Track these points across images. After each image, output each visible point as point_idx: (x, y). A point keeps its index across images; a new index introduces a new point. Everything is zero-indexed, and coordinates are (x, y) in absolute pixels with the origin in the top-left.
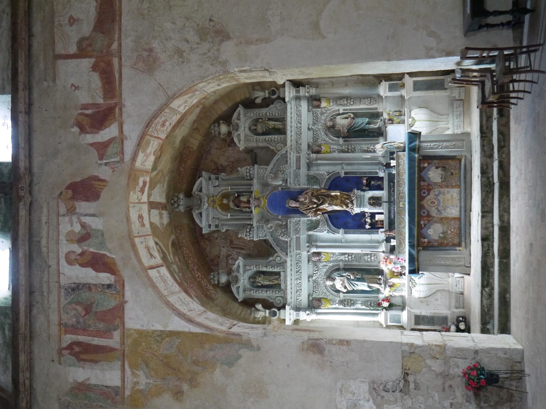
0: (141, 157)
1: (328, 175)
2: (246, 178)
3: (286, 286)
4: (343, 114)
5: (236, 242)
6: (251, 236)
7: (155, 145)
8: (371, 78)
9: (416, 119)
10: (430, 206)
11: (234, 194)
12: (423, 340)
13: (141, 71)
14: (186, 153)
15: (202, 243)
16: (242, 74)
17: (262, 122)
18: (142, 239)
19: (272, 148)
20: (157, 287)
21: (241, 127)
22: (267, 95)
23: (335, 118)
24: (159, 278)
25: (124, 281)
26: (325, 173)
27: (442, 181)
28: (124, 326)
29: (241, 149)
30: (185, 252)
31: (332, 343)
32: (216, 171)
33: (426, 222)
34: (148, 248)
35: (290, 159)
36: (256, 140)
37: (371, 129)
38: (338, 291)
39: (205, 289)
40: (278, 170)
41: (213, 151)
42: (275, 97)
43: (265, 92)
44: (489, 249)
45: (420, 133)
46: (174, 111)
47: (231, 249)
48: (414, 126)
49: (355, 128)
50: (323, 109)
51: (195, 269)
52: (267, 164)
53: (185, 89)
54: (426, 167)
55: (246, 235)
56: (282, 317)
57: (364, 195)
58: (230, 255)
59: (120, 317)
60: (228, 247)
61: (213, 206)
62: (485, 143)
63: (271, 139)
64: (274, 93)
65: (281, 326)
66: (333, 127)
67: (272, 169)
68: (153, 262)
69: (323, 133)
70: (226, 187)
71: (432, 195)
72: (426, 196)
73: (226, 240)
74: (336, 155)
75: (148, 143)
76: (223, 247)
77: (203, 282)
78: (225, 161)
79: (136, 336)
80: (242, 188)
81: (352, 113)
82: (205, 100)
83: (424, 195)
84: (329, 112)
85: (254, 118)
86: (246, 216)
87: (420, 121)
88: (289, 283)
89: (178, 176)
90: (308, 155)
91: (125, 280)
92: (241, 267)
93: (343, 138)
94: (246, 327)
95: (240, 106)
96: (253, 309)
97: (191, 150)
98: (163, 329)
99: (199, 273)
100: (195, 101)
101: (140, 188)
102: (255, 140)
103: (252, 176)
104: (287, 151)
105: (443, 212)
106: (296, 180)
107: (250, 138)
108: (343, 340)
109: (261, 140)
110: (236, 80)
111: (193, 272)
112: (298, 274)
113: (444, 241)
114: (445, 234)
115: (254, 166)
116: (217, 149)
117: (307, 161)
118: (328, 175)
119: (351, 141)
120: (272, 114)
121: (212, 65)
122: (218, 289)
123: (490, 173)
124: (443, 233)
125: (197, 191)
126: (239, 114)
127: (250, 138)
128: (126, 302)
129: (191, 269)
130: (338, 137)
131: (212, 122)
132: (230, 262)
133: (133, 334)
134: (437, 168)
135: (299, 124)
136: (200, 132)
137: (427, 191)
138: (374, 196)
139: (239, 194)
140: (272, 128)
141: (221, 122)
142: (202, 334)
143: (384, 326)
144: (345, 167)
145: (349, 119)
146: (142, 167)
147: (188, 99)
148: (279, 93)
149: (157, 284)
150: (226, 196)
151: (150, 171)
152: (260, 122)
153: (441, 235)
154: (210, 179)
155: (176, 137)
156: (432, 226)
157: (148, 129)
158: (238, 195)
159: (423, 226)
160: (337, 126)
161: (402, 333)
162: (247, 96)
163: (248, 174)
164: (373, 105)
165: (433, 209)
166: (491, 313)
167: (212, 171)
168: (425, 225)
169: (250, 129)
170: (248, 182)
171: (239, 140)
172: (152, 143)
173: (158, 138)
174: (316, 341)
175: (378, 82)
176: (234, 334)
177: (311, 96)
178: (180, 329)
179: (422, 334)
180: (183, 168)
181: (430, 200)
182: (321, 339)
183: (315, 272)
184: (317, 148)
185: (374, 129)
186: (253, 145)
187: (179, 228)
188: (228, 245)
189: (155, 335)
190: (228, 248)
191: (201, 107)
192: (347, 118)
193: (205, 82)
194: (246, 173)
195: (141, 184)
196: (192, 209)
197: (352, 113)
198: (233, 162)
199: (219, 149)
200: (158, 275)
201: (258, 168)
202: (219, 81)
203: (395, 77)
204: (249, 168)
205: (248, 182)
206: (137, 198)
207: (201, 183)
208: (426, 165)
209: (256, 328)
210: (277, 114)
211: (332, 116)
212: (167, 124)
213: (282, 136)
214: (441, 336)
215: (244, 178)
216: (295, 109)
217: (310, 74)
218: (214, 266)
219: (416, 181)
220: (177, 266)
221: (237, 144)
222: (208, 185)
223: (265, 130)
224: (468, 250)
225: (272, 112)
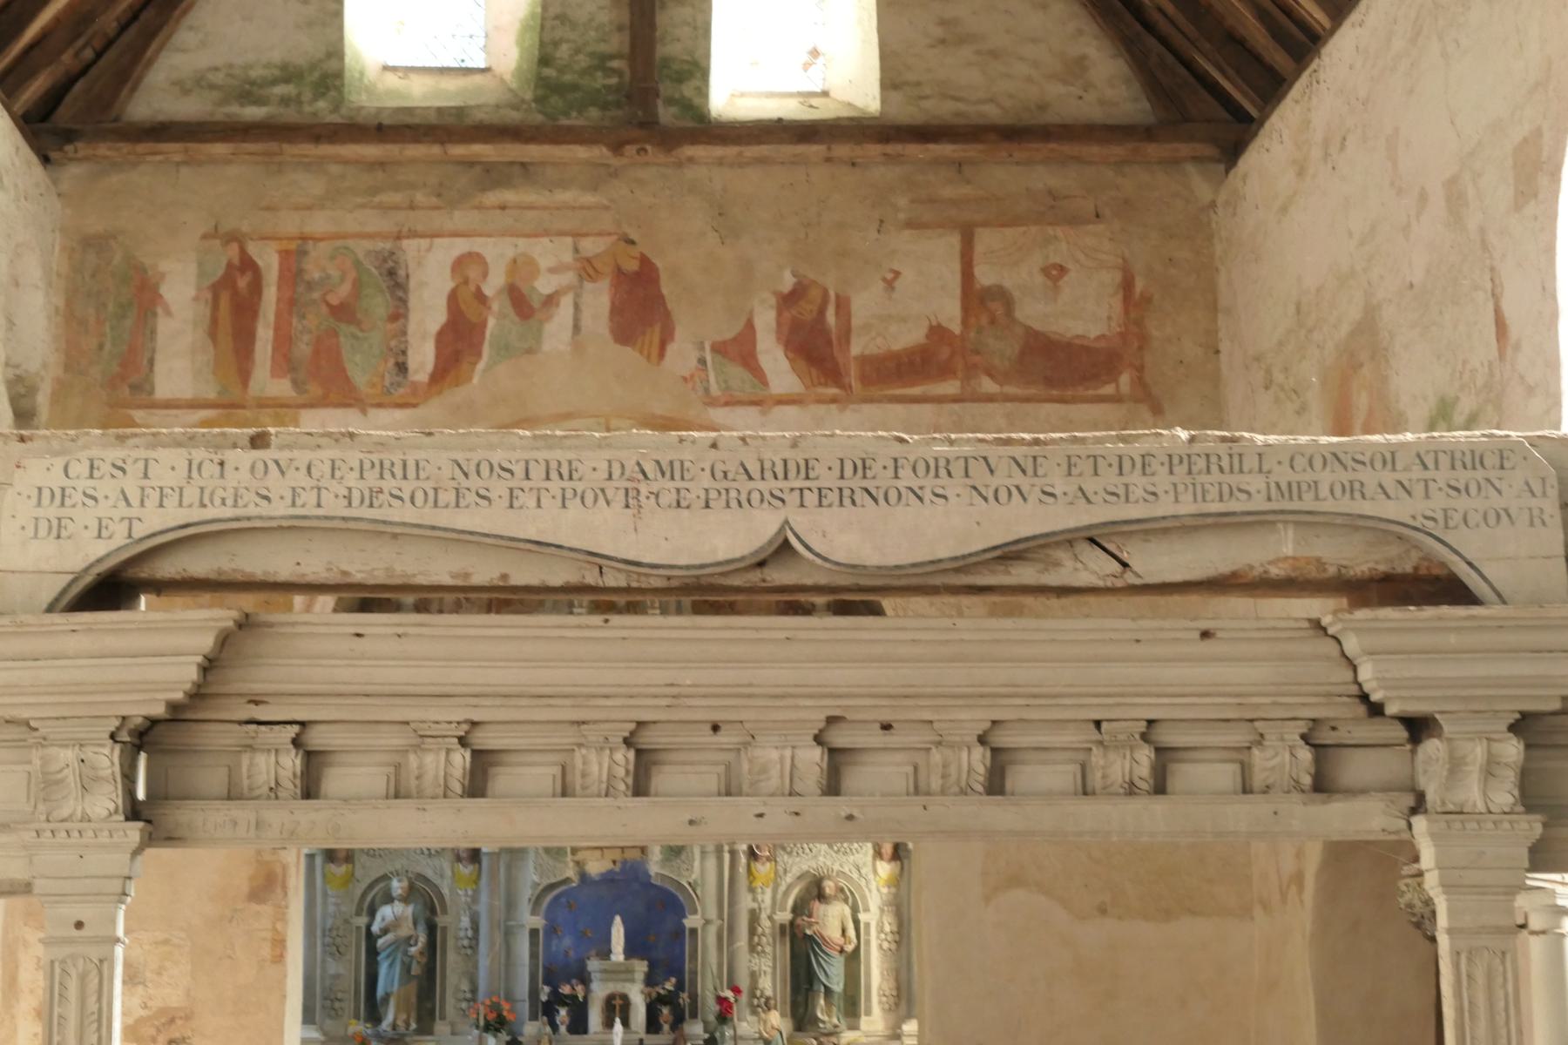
25: (415, 406)
69: (805, 868)
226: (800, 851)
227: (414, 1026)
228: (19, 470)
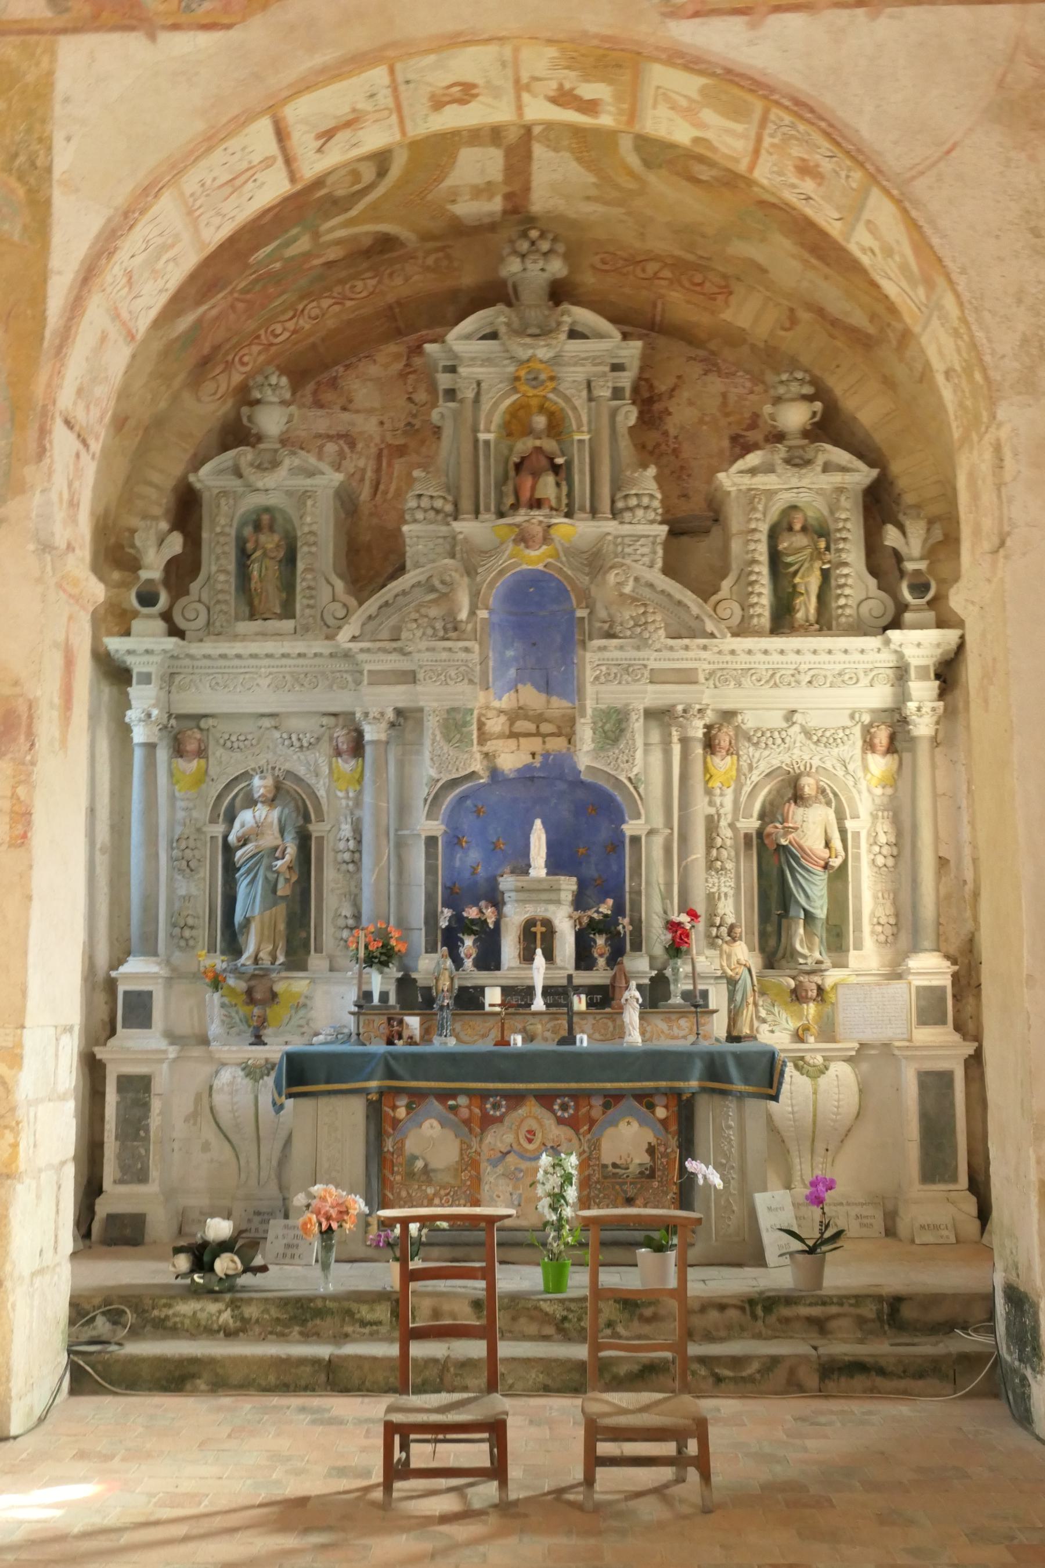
0: (689, 84)
1: (630, 779)
2: (619, 495)
3: (244, 638)
4: (843, 832)
5: (399, 465)
6: (420, 515)
7: (730, 140)
8: (970, 925)
9: (823, 1080)
10: (519, 1127)
11: (563, 454)
12: (38, 1101)
13: (1004, 75)
14: (708, 284)
15: (392, 348)
16: (988, 455)
17: (817, 549)
18: (385, 98)
19: (726, 584)
20: (209, 150)
21: (800, 478)
22: (910, 566)
23: (828, 804)
24: (244, 165)
25: (228, 27)
26: (635, 770)
27: (605, 1166)
28: (64, 31)
29: (721, 476)
30: (360, 284)
31: (20, 782)
32: (646, 395)
33: (464, 1113)
34: (352, 122)
35: (687, 648)
36: (754, 530)
37: (789, 927)
38: (231, 818)
39: (230, 358)
40: (645, 605)
41: (716, 385)
42: (907, 596)
43: (922, 558)
44: (364, 1324)
45: (775, 1098)
46: (854, 211)
47: (373, 450)
48: (796, 1073)
49: (793, 871)
50: (859, 763)
51: (301, 322)
52: (669, 570)
53: (935, 241)
54: (653, 1113)
55: (420, 496)
56: (136, 625)
57: (558, 902)
58: (352, 445)
59: (96, 16)
60: (383, 441)
61: (517, 379)
62: (733, 1314)
63: (756, 581)
64: (920, 588)
65: (83, 607)
66: (798, 797)
67: (651, 586)
68: (303, 141)
69: (776, 763)
70: (590, 422)
71: (557, 1132)
72: (553, 1112)
73: (405, 433)
74: (701, 808)
75: (736, 112)
76: (382, 423)
77: (255, 349)
79: (30, 78)
80: (582, 482)
81: (845, 862)
82: (894, 343)
83: (556, 1107)
84: (850, 782)
85: (830, 521)
86: (487, 495)
87: (815, 1093)
88: (254, 647)
90: (700, 711)
91: (232, 33)
92: (309, 481)
93: (760, 833)
94: (76, 484)
95: (874, 473)
96: (164, 526)
98: (57, 173)
99: (286, 335)
100: (890, 289)
101: (573, 89)
102: (753, 526)
103: (627, 516)
104: (712, 635)
105: (500, 1169)
106: (614, 670)
107: (760, 507)
108: (29, 824)
109: (752, 546)
110: (965, 439)
111: (291, 314)
112: (288, 677)
113: (398, 1173)
114: (423, 1178)
115: (661, 523)
116: (724, 395)
117: (680, 708)
118: (630, 779)
119: (748, 857)
121: (1025, 341)
122: (230, 403)
123: (626, 1328)
124: (426, 1170)
125: (574, 323)
126: (844, 469)
127: (760, 507)
128: (152, 37)
129: (300, 307)
130: (762, 816)
131: (817, 372)
132: (331, 448)
133: (37, 64)
134: (651, 1150)
135: (808, 679)
136: (783, 333)
137: (571, 1116)
138: (557, 936)
139: (563, 474)
140: (794, 586)
141: (818, 406)
142: (41, 319)
143: (113, 974)
144: (658, 841)
145: (825, 853)
146: (648, 93)
147: (897, 258)
148: (918, 609)
149: (218, 156)
150: (556, 427)
151: (637, 128)
152: (815, 544)
153: (419, 1164)
154: (617, 368)
155: (763, 240)
156: (449, 1134)
157: (787, 108)
158: (560, 466)
159: (451, 1102)
160: (800, 811)
161: (69, 1029)
162: (909, 499)
163: (633, 502)
164: (873, 932)
165: (509, 1138)
166: (148, 1328)
167: (647, 380)
168: (453, 1109)
169: (794, 508)
170: (605, 504)
171: (753, 471)
172: (739, 128)
173: (756, 152)
174: (23, 729)
175: (952, 950)
176: (44, 432)
177: (904, 721)
178: (58, 238)
179: (63, 1098)
180: (656, 273)
181: (541, 1125)
182: (33, 745)
183: (294, 737)
185: (790, 938)
186: (736, 521)
187: (445, 263)
188: (389, 439)
189: (35, 146)
190: (377, 440)
191: (871, 330)
192: (827, 845)
193: (963, 320)
194: (636, 495)
195: (589, 91)
196: (509, 304)
197: (845, 862)
198: (676, 452)
199: (725, 403)
200: (256, 159)
201: (656, 536)
202: (964, 369)
203: (969, 1009)
204: (656, 504)
205: (605, 504)
206: (537, 74)
207: (600, 336)
208: (661, 1113)
209: (73, 520)
210: (842, 601)
211: (835, 794)
212: (808, 186)
213: (765, 621)
214: (56, 1161)
215: (619, 489)
217: (986, 701)
218: (315, 393)
219: (608, 1085)
220: (307, 256)
221: (740, 464)
222: (595, 361)
223: (789, 559)
224: (371, 1252)
225: (851, 586)
227: (281, 959)
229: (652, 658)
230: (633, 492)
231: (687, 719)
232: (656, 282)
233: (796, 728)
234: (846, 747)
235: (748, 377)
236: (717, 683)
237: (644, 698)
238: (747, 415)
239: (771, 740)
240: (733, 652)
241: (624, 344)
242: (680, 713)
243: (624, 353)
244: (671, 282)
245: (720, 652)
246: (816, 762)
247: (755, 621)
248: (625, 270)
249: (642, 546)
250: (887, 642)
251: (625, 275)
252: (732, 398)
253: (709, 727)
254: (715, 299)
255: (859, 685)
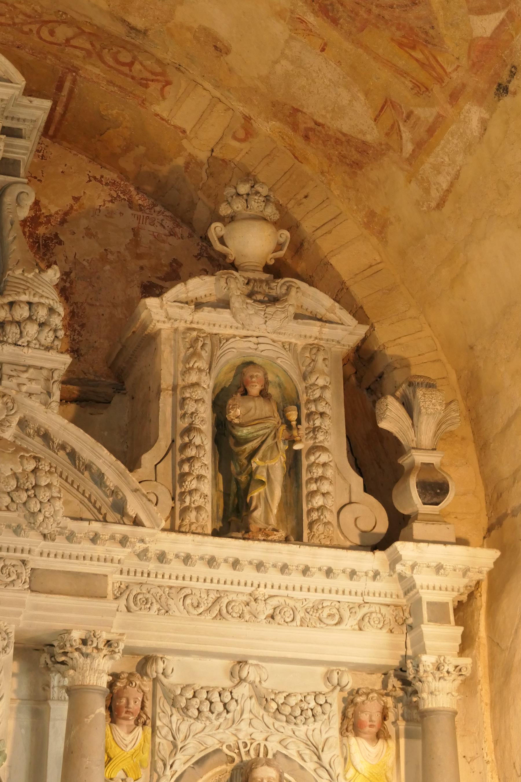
14: (137, 67)
35: (95, 539)
50: (337, 751)
69: (212, 744)
78: (76, 262)
82: (408, 148)
89: (28, 11)
90: (108, 643)
95: (362, 330)
97: (154, 88)
104: (137, 522)
116: (136, 232)
117: (77, 635)
120: (322, 478)
127: (205, 354)
140: (251, 474)
163: (22, 312)
180: (68, 40)
184: (135, 706)
194: (30, 304)
199: (136, 241)
201: (52, 371)
204: (57, 321)
210: (318, 501)
216: (346, 598)
226: (206, 708)
228: (343, 574)
229: (37, 550)
230: (24, 298)
231: (86, 655)
232: (67, 49)
233: (244, 690)
234: (318, 725)
235: (168, 213)
236: (132, 604)
237: (19, 614)
238: (165, 261)
239: (206, 708)
240: (162, 557)
241: (25, 100)
242: (77, 644)
243: (23, 113)
244: (89, 54)
245: (143, 555)
246: (273, 746)
247: (192, 516)
248: (26, 28)
249: (30, 380)
250: (396, 560)
251: (26, 33)
252: (146, 237)
253: (115, 677)
254: (146, 86)
255: (342, 626)
